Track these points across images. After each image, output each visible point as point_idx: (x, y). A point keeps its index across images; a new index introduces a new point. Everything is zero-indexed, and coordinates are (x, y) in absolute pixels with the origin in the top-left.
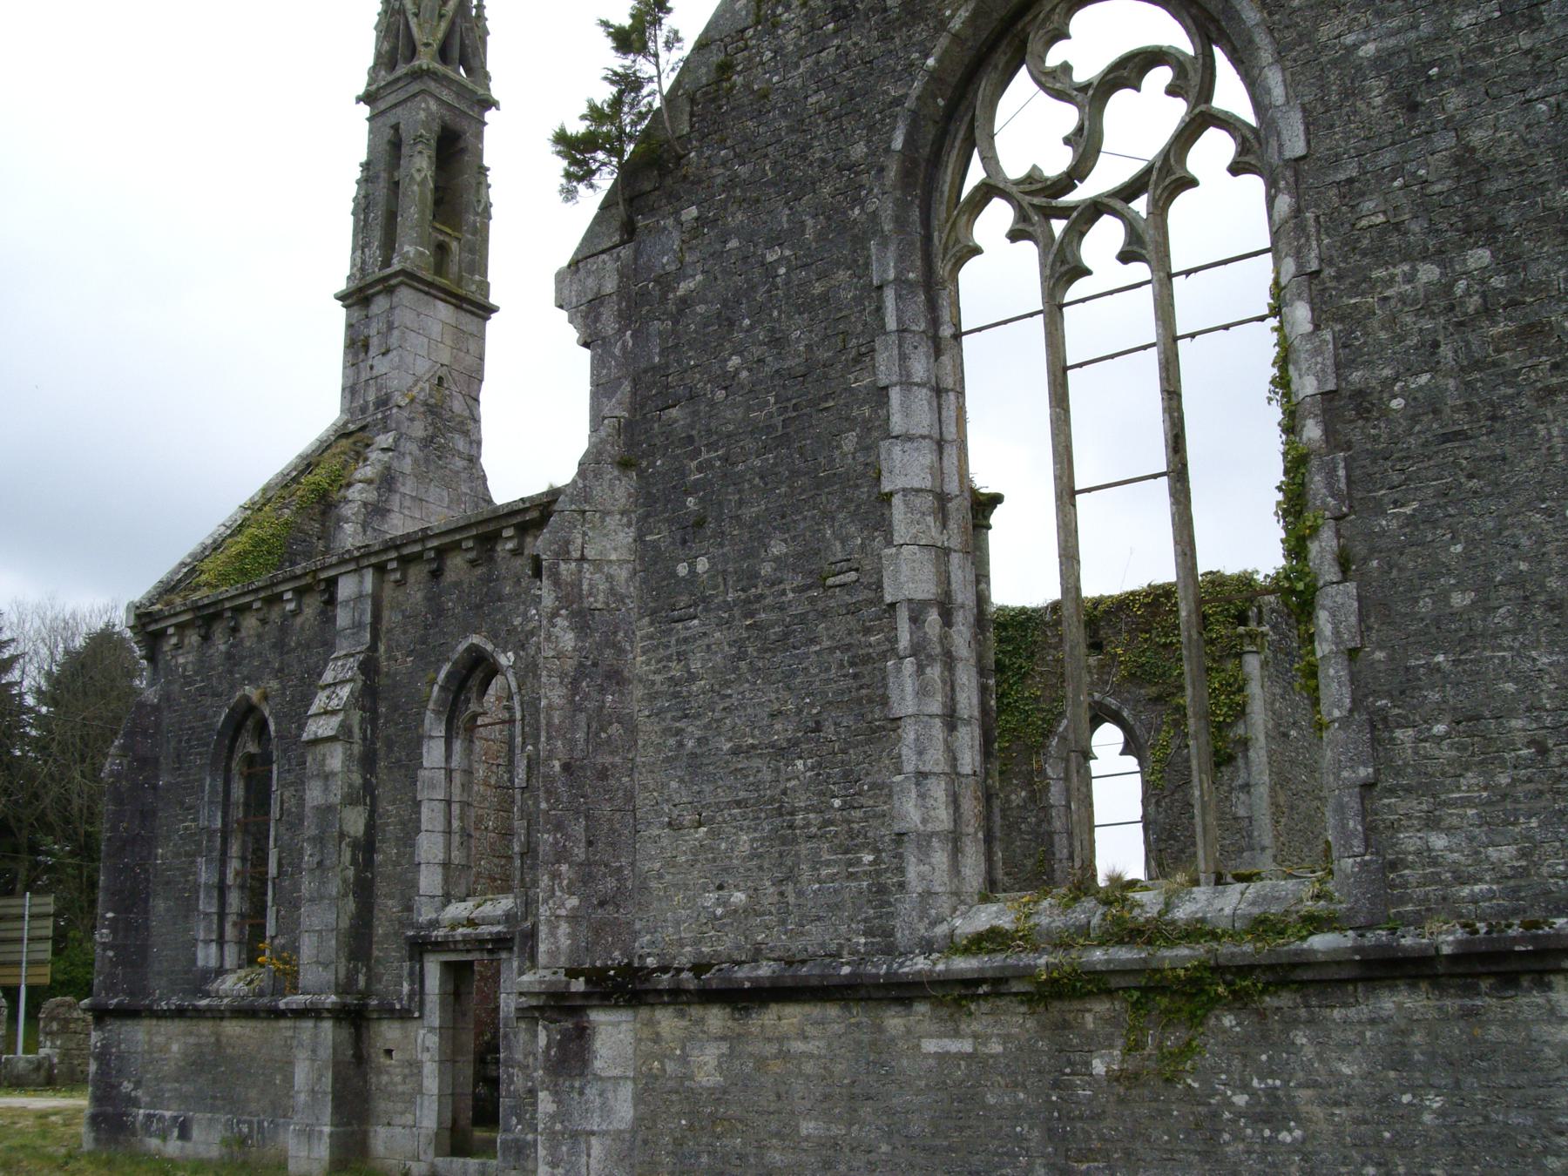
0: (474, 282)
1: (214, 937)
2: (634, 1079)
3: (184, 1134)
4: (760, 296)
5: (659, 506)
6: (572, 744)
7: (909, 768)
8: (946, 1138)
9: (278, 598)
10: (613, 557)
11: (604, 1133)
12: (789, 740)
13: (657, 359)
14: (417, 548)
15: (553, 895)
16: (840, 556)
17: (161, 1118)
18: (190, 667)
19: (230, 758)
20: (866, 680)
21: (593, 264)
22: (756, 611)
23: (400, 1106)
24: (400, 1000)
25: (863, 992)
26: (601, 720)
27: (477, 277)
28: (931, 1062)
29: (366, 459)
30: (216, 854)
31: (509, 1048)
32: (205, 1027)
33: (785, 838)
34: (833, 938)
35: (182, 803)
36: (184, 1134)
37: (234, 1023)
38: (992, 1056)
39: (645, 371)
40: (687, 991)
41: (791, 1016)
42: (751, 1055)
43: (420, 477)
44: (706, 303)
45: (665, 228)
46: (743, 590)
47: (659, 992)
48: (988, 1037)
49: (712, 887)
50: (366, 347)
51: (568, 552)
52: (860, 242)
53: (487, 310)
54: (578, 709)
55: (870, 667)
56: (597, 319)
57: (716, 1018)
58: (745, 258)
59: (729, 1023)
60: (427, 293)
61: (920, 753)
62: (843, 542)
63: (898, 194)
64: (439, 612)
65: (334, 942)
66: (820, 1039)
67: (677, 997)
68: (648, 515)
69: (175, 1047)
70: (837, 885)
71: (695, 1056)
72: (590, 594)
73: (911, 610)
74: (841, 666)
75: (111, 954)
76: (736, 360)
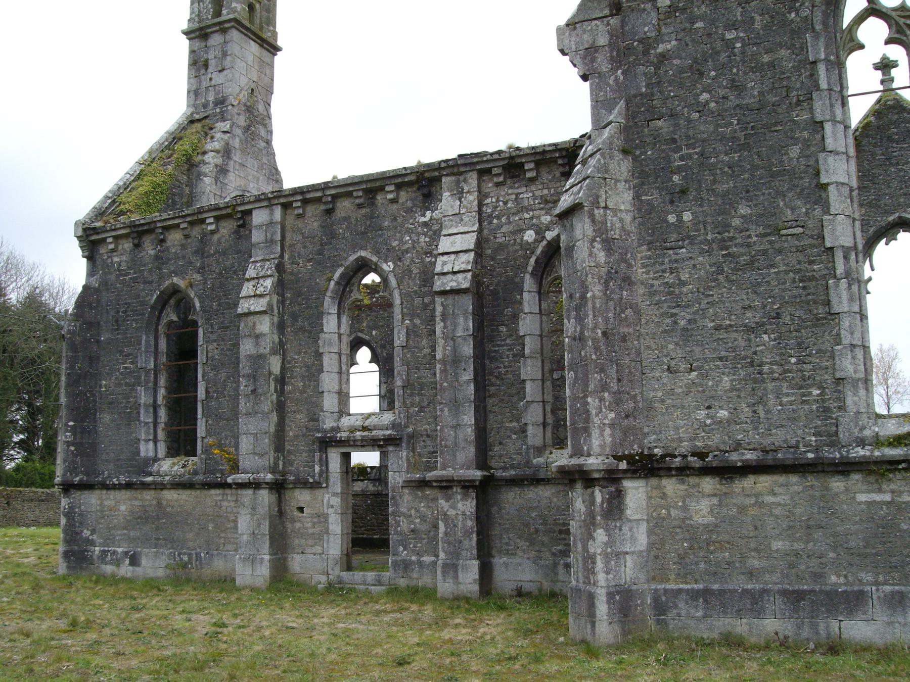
0: (269, 31)
1: (151, 438)
2: (647, 521)
3: (134, 561)
4: (723, 57)
5: (651, 180)
6: (607, 319)
7: (846, 341)
8: (874, 548)
9: (203, 221)
10: (622, 208)
11: (633, 553)
12: (757, 323)
13: (644, 90)
14: (319, 194)
15: (601, 411)
16: (790, 218)
17: (114, 553)
18: (124, 264)
19: (157, 325)
20: (812, 290)
21: (587, 26)
22: (730, 246)
23: (310, 542)
24: (313, 477)
25: (820, 468)
26: (621, 306)
27: (271, 28)
28: (863, 506)
29: (212, 138)
30: (151, 385)
31: (396, 505)
32: (149, 496)
33: (758, 379)
34: (802, 437)
35: (121, 352)
36: (134, 561)
37: (172, 492)
38: (904, 503)
39: (635, 96)
40: (693, 468)
41: (765, 482)
42: (735, 504)
43: (243, 151)
44: (681, 59)
45: (645, 10)
46: (718, 233)
47: (669, 469)
48: (900, 493)
49: (702, 407)
50: (206, 66)
51: (598, 203)
52: (797, 33)
53: (274, 49)
54: (609, 299)
55: (814, 283)
56: (593, 60)
57: (708, 484)
58: (709, 35)
59: (718, 486)
60: (246, 35)
61: (852, 334)
62: (793, 209)
63: (823, 7)
64: (333, 235)
65: (267, 440)
66: (785, 495)
67: (683, 471)
68: (643, 184)
69: (123, 508)
70: (794, 407)
71: (692, 505)
72: (612, 230)
73: (844, 252)
74: (794, 281)
75: (72, 448)
76: (705, 96)
